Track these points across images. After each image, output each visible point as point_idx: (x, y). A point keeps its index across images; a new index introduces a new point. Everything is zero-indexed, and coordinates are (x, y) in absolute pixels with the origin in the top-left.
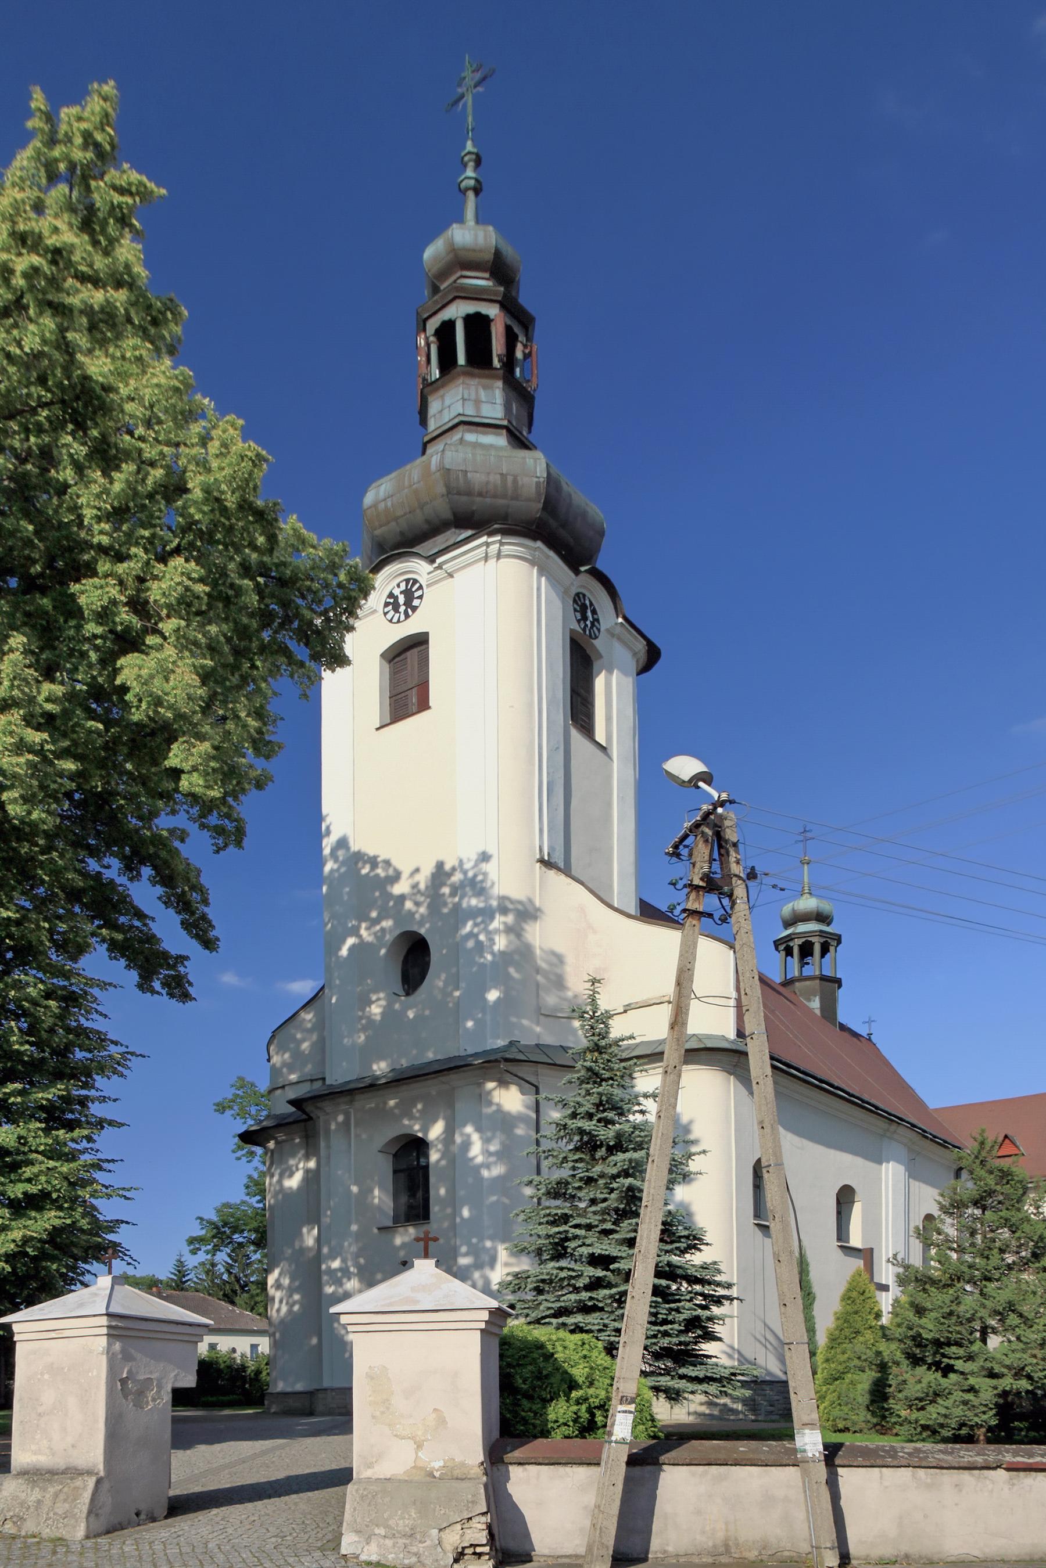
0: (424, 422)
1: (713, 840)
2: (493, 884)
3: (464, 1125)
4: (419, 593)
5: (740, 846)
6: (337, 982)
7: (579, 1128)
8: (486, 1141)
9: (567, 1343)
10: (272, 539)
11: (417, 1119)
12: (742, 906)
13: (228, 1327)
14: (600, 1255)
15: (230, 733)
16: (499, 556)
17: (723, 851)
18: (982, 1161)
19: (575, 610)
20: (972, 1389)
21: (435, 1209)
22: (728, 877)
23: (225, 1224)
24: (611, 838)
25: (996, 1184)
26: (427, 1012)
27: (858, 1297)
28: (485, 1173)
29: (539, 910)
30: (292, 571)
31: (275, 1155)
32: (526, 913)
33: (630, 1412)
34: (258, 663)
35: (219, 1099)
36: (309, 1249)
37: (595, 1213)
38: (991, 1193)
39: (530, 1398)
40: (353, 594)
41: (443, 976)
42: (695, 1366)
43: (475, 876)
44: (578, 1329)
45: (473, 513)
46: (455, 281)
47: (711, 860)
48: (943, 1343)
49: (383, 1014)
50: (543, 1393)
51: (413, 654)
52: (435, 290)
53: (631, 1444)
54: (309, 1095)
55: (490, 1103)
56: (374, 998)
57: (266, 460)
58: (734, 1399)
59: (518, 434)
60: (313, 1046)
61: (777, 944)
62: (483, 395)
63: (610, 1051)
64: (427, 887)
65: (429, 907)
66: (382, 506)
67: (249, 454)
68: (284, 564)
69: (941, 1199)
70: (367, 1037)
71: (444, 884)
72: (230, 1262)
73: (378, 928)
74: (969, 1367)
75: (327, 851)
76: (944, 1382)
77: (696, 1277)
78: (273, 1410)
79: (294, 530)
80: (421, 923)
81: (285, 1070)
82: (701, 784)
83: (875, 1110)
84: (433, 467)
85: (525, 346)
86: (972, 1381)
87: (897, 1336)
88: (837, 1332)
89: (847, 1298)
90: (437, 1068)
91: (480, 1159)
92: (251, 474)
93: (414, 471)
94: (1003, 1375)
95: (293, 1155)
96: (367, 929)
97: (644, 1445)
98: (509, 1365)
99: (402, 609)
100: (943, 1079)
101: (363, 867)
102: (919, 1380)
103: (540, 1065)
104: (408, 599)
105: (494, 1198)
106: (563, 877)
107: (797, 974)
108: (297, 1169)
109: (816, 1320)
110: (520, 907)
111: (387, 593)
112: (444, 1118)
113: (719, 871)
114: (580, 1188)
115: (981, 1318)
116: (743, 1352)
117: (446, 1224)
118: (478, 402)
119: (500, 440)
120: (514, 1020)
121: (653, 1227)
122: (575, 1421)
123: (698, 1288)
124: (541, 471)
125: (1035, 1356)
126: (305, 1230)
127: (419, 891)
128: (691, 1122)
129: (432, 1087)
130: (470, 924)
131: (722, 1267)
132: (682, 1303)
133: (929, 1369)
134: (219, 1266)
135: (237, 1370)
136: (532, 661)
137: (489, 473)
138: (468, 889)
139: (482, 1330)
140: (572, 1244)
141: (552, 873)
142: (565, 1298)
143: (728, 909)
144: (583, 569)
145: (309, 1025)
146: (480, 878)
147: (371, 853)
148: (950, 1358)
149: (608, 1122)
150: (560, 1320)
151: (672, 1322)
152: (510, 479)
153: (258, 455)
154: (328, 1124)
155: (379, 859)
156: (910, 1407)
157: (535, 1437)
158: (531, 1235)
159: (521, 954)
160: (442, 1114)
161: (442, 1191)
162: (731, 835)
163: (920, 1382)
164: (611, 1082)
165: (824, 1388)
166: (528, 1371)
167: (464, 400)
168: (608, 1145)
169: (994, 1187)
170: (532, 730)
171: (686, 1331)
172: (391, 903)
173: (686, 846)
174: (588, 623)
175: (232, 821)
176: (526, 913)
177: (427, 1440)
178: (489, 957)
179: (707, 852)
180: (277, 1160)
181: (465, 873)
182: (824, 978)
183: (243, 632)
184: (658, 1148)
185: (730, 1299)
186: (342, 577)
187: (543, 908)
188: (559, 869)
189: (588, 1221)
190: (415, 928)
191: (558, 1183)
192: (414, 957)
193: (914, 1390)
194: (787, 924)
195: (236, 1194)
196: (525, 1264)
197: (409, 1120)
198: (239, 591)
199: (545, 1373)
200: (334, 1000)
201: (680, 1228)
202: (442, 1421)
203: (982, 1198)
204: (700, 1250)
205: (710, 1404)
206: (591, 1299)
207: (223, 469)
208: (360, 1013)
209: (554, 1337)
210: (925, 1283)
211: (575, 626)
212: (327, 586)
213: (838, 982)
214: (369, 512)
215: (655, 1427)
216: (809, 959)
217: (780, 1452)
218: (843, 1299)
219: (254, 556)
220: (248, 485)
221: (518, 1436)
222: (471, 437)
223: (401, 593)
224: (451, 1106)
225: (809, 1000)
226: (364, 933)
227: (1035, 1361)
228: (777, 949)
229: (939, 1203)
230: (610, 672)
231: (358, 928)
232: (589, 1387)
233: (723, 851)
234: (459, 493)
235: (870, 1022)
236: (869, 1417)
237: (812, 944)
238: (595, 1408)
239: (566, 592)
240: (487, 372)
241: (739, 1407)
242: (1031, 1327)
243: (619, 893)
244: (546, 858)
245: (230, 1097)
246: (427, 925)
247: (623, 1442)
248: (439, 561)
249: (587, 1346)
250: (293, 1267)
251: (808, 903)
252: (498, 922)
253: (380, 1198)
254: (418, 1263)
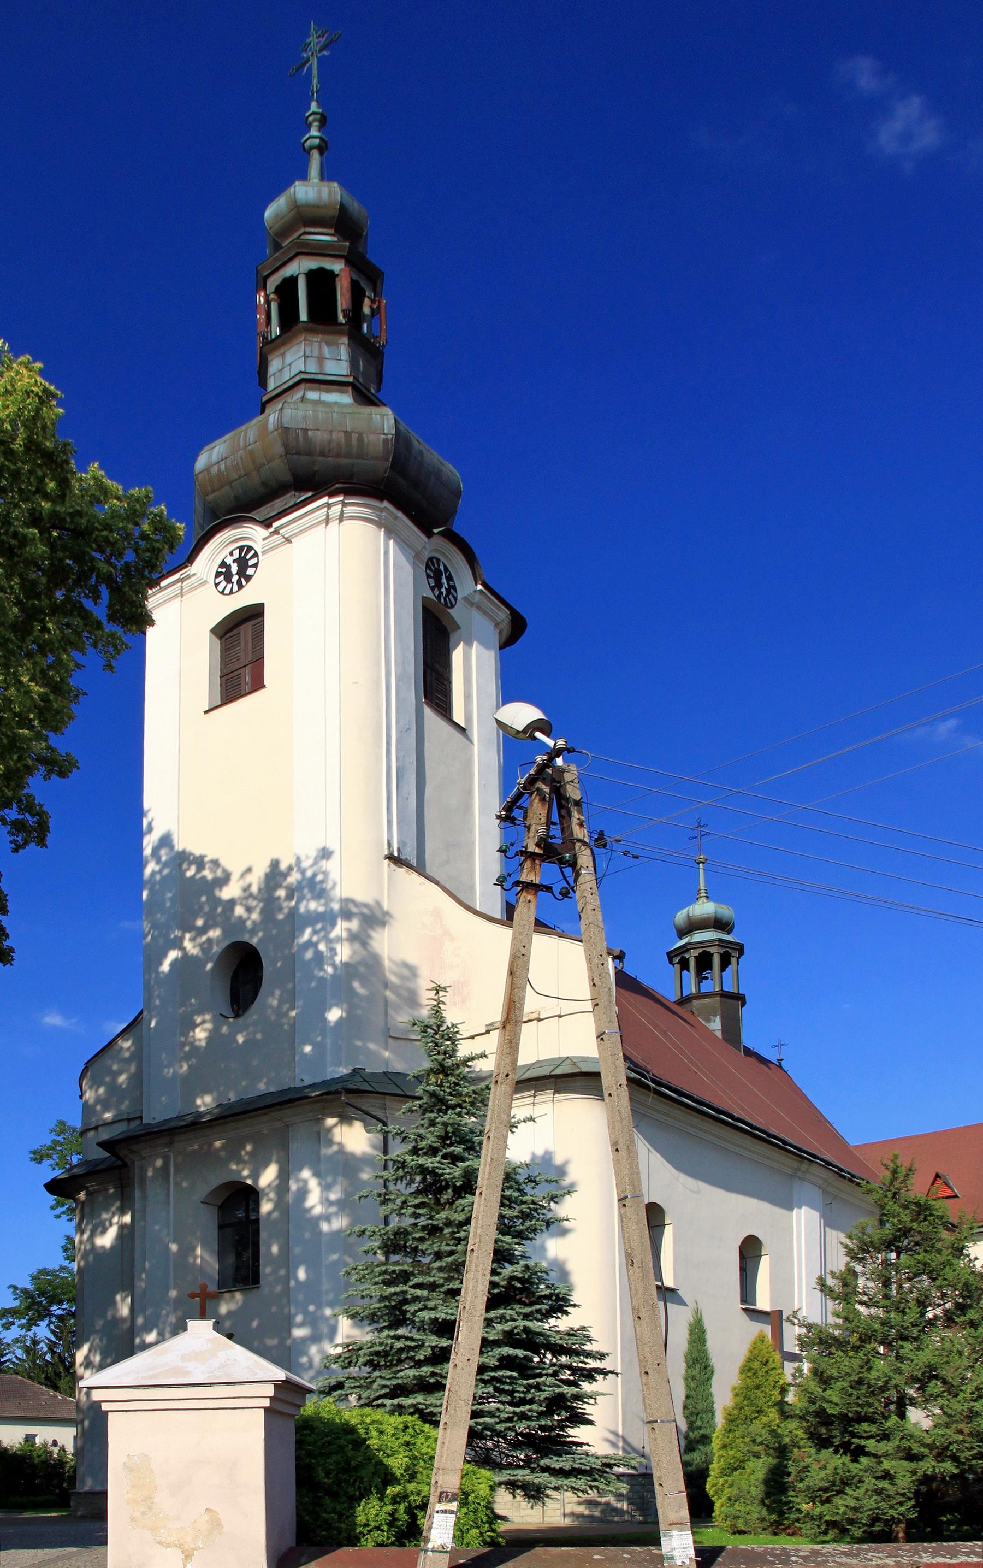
0: (263, 382)
1: (551, 799)
2: (335, 884)
3: (300, 1170)
4: (254, 561)
5: (584, 805)
6: (157, 1002)
7: (421, 1166)
8: (326, 1188)
9: (384, 1427)
10: (64, 484)
11: (244, 1162)
12: (588, 877)
13: (49, 1415)
14: (443, 1320)
15: (11, 701)
16: (341, 518)
17: (563, 812)
18: (895, 1194)
19: (428, 576)
20: (886, 1476)
21: (266, 1270)
22: (570, 841)
23: (42, 1293)
24: (472, 831)
25: (912, 1221)
26: (259, 1036)
27: (757, 1367)
28: (325, 1227)
29: (387, 914)
30: (88, 521)
31: (87, 1210)
32: (373, 918)
33: (452, 1512)
34: (50, 626)
35: (36, 1146)
36: (123, 1320)
37: (440, 1269)
38: (906, 1232)
39: (334, 1496)
40: (157, 545)
41: (278, 993)
42: (560, 1456)
43: (315, 875)
44: (400, 1409)
45: (315, 473)
46: (298, 237)
47: (549, 823)
48: (852, 1420)
49: (209, 1039)
50: (351, 1489)
51: (247, 629)
52: (277, 247)
53: (453, 1552)
54: (121, 1137)
55: (330, 1142)
56: (199, 1020)
57: (54, 396)
58: (613, 1495)
59: (364, 390)
60: (129, 1079)
61: (670, 955)
62: (326, 350)
63: (457, 1072)
64: (260, 890)
65: (262, 912)
66: (214, 470)
67: (36, 389)
68: (79, 514)
69: (848, 1242)
70: (190, 1067)
71: (279, 886)
72: (54, 1339)
73: (204, 938)
74: (883, 1447)
75: (147, 851)
76: (854, 1467)
77: (561, 1346)
78: (79, 1514)
79: (95, 478)
80: (253, 932)
81: (99, 1107)
82: (538, 735)
83: (782, 1146)
84: (271, 427)
85: (373, 301)
86: (886, 1464)
87: (798, 1412)
88: (735, 1412)
89: (747, 1370)
90: (269, 1101)
91: (318, 1210)
92: (38, 410)
93: (249, 432)
94: (923, 1457)
95: (107, 1210)
96: (192, 940)
97: (474, 1554)
98: (310, 1454)
99: (235, 579)
100: (866, 1115)
101: (188, 869)
102: (821, 1465)
103: (388, 1097)
104: (241, 569)
105: (335, 1257)
106: (415, 875)
107: (694, 991)
108: (111, 1225)
109: (715, 1399)
110: (365, 911)
111: (219, 562)
112: (278, 1162)
113: (559, 834)
114: (422, 1240)
115: (896, 1386)
116: (630, 1440)
117: (279, 1288)
118: (321, 359)
119: (345, 398)
120: (359, 1043)
121: (480, 1277)
122: (390, 1524)
123: (564, 1359)
124: (389, 429)
125: (960, 1432)
126: (118, 1298)
127: (251, 895)
128: (566, 1163)
129: (264, 1125)
130: (308, 931)
131: (592, 1333)
132: (544, 1378)
133: (836, 1452)
134: (42, 1345)
135: (54, 1466)
136: (379, 633)
137: (331, 432)
138: (306, 891)
139: (266, 1409)
140: (412, 1308)
141: (402, 871)
142: (402, 1374)
143: (571, 880)
144: (436, 531)
145: (127, 1055)
146: (320, 877)
147: (197, 853)
148: (860, 1437)
149: (455, 1159)
150: (396, 1401)
151: (531, 1402)
152: (355, 436)
153: (45, 390)
154: (143, 1170)
155: (206, 859)
156: (813, 1500)
157: (340, 1545)
158: (363, 1297)
159: (368, 967)
160: (274, 1157)
161: (275, 1249)
162: (573, 792)
163: (825, 1467)
164: (459, 1109)
165: (721, 1481)
166: (331, 1462)
167: (306, 357)
168: (455, 1186)
169: (908, 1225)
170: (379, 710)
171: (549, 1413)
172: (219, 910)
173: (520, 807)
174: (443, 590)
175: (33, 816)
176: (373, 918)
177: (198, 1548)
178: (330, 970)
179: (544, 812)
180: (89, 1216)
181: (303, 872)
182: (724, 995)
183: (30, 589)
184: (486, 1177)
185: (604, 1372)
186: (146, 527)
187: (392, 912)
188: (410, 867)
189: (432, 1279)
190: (246, 938)
191: (395, 1234)
192: (243, 972)
193: (817, 1478)
194: (682, 933)
195: (54, 1260)
196: (364, 1335)
197: (237, 1164)
198: (24, 541)
199: (353, 1463)
200: (153, 1024)
201: (542, 1286)
202: (216, 1524)
203: (896, 1239)
204: (567, 1313)
205: (590, 1503)
206: (433, 1374)
207: (8, 407)
208: (183, 1039)
209: (368, 1420)
210: (831, 1345)
211: (429, 594)
212: (127, 536)
213: (741, 999)
214: (201, 476)
215: (494, 1531)
216: (707, 974)
217: (644, 1560)
218: (742, 1371)
219: (46, 505)
220: (35, 424)
221: (320, 1544)
222: (313, 395)
223: (234, 561)
224: (284, 1146)
225: (709, 1021)
226: (187, 944)
227: (961, 1438)
228: (671, 962)
229: (846, 1246)
230: (469, 644)
231: (182, 939)
232: (409, 1482)
233: (563, 812)
234: (298, 453)
235: (779, 1046)
236: (764, 1513)
237: (710, 955)
238: (417, 1507)
239: (417, 556)
240: (329, 328)
241: (625, 1506)
242: (957, 1395)
243: (482, 894)
244: (396, 854)
245: (49, 1143)
246: (260, 934)
247: (442, 1550)
248: (275, 525)
249: (410, 1431)
250: (105, 1342)
251: (704, 908)
252: (340, 929)
253: (202, 1258)
254: (191, 1324)
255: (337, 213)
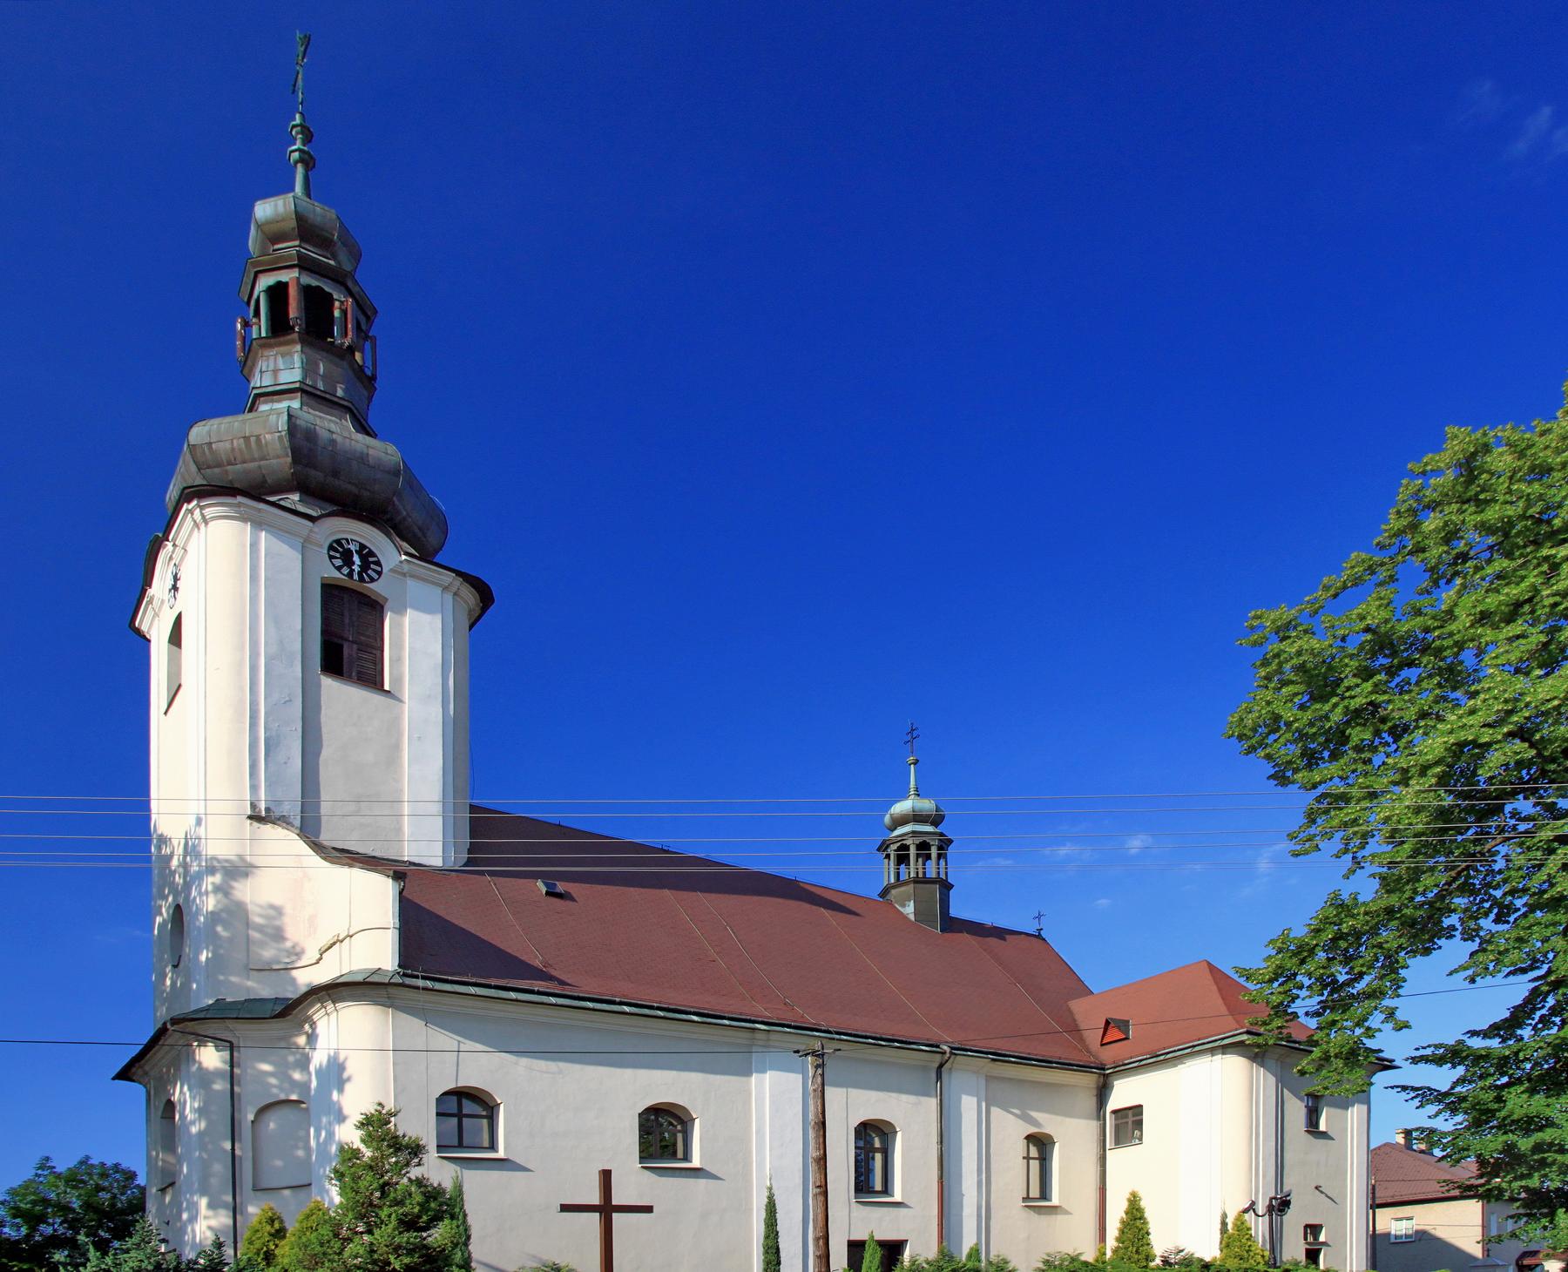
16: (206, 522)
32: (238, 870)
159: (235, 913)
225: (904, 906)
255: (294, 224)
